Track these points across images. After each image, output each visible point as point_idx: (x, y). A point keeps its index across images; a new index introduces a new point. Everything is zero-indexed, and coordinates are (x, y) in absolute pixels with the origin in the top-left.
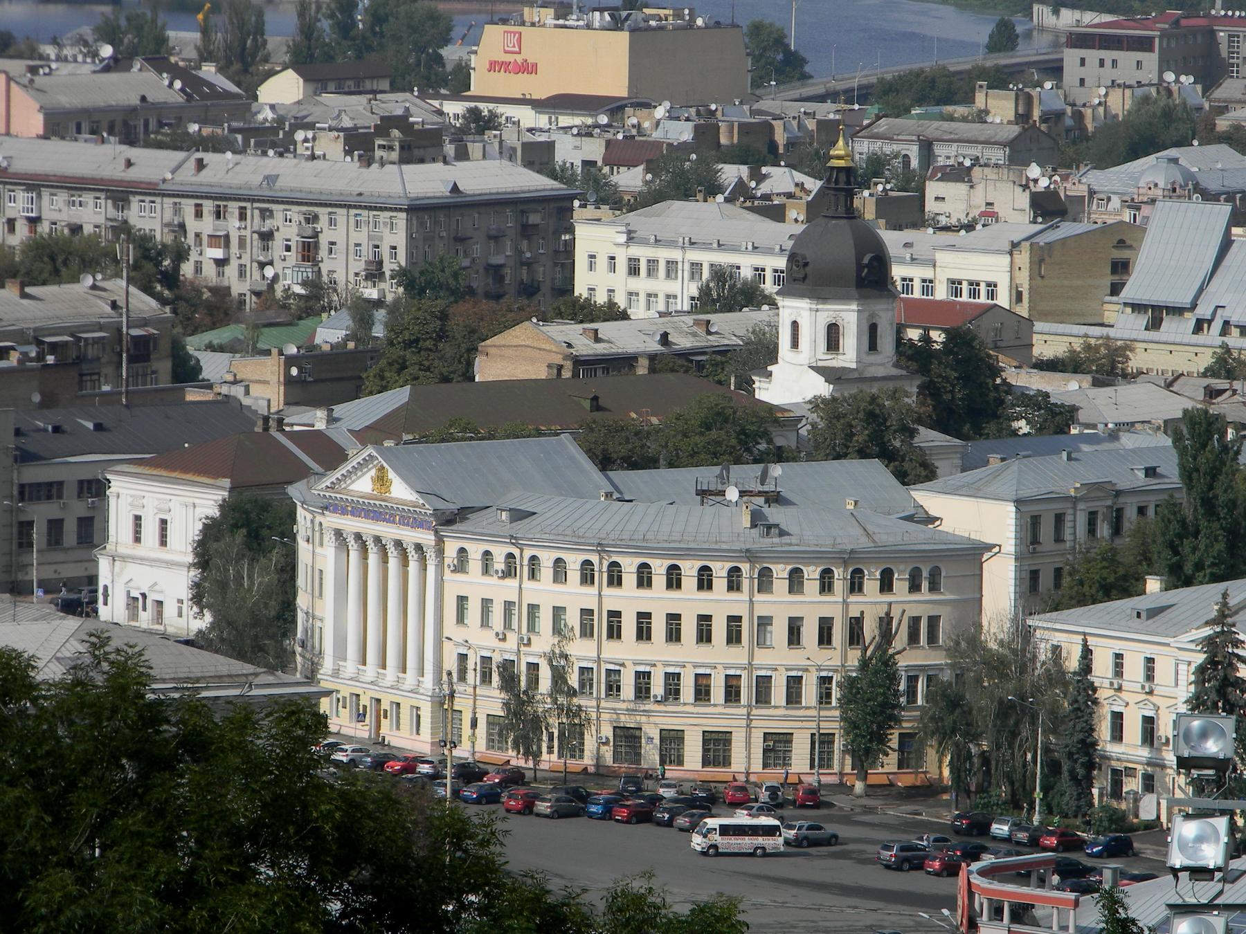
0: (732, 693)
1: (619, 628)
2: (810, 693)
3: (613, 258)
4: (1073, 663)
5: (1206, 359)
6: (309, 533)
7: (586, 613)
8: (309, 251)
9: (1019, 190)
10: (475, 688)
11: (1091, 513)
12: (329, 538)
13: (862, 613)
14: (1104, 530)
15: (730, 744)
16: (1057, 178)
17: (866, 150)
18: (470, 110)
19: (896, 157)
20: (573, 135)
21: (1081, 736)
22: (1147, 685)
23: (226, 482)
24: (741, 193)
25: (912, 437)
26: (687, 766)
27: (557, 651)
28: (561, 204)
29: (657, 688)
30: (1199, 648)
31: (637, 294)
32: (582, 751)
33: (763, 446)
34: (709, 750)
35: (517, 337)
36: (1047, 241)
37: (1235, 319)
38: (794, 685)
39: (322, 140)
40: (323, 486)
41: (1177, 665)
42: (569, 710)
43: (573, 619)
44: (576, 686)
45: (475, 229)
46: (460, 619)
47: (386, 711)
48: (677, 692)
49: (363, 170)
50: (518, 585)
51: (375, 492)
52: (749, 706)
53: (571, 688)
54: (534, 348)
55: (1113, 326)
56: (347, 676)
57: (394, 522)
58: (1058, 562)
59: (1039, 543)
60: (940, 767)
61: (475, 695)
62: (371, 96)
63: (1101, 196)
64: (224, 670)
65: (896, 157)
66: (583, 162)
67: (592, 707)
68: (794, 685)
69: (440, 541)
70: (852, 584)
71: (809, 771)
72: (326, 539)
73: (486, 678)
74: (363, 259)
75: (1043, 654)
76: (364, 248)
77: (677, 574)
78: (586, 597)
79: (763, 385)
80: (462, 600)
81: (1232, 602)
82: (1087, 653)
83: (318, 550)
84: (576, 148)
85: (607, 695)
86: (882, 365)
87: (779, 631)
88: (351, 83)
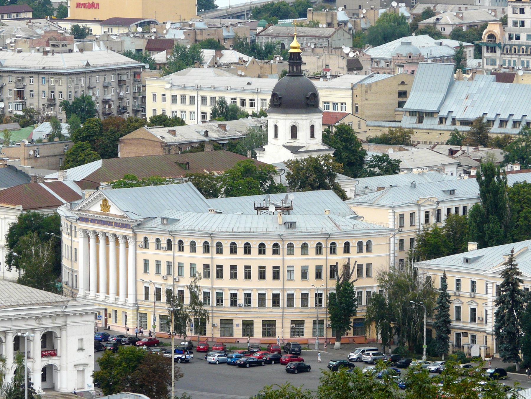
0: (276, 302)
1: (222, 273)
2: (312, 301)
3: (164, 95)
4: (438, 285)
5: (447, 136)
6: (69, 231)
7: (207, 266)
8: (20, 94)
9: (341, 59)
10: (154, 303)
11: (426, 212)
12: (80, 234)
13: (337, 263)
14: (432, 220)
15: (275, 326)
16: (357, 52)
17: (264, 41)
18: (74, 26)
19: (278, 44)
20: (131, 38)
21: (444, 318)
22: (472, 294)
23: (20, 207)
24: (215, 65)
25: (334, 178)
26: (255, 336)
27: (194, 285)
28: (135, 70)
29: (241, 300)
30: (500, 276)
31: (185, 112)
32: (205, 331)
33: (269, 183)
34: (265, 329)
35: (138, 134)
36: (368, 83)
37: (458, 117)
38: (305, 297)
39: (19, 43)
40: (77, 209)
41: (487, 284)
42: (200, 312)
43: (200, 269)
44: (202, 300)
45: (97, 83)
46: (146, 270)
47: (110, 314)
48: (250, 302)
49: (45, 57)
50: (211, 257)
51: (102, 212)
52: (283, 308)
53: (200, 302)
54: (146, 139)
55: (400, 122)
56: (91, 298)
57: (112, 225)
58: (414, 235)
59: (403, 227)
60: (377, 335)
61: (155, 306)
62: (28, 21)
63: (375, 60)
64: (47, 300)
65: (278, 44)
66: (136, 49)
67: (210, 310)
68: (305, 297)
69: (135, 235)
70: (317, 250)
71: (312, 337)
72: (78, 234)
73: (158, 297)
74: (46, 98)
75: (421, 279)
76: (47, 93)
77: (249, 247)
78: (206, 259)
79: (262, 155)
80: (146, 262)
81: (515, 253)
82: (444, 279)
83: (74, 239)
84: (132, 43)
85: (217, 305)
86: (316, 144)
87: (298, 274)
88: (14, 15)
